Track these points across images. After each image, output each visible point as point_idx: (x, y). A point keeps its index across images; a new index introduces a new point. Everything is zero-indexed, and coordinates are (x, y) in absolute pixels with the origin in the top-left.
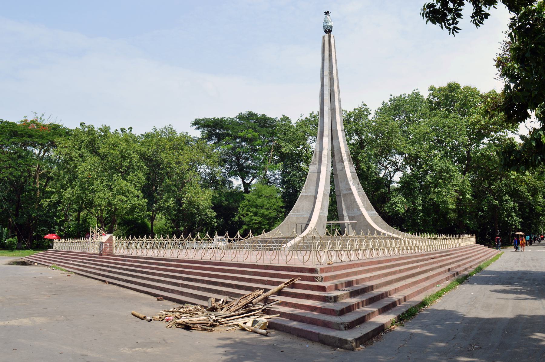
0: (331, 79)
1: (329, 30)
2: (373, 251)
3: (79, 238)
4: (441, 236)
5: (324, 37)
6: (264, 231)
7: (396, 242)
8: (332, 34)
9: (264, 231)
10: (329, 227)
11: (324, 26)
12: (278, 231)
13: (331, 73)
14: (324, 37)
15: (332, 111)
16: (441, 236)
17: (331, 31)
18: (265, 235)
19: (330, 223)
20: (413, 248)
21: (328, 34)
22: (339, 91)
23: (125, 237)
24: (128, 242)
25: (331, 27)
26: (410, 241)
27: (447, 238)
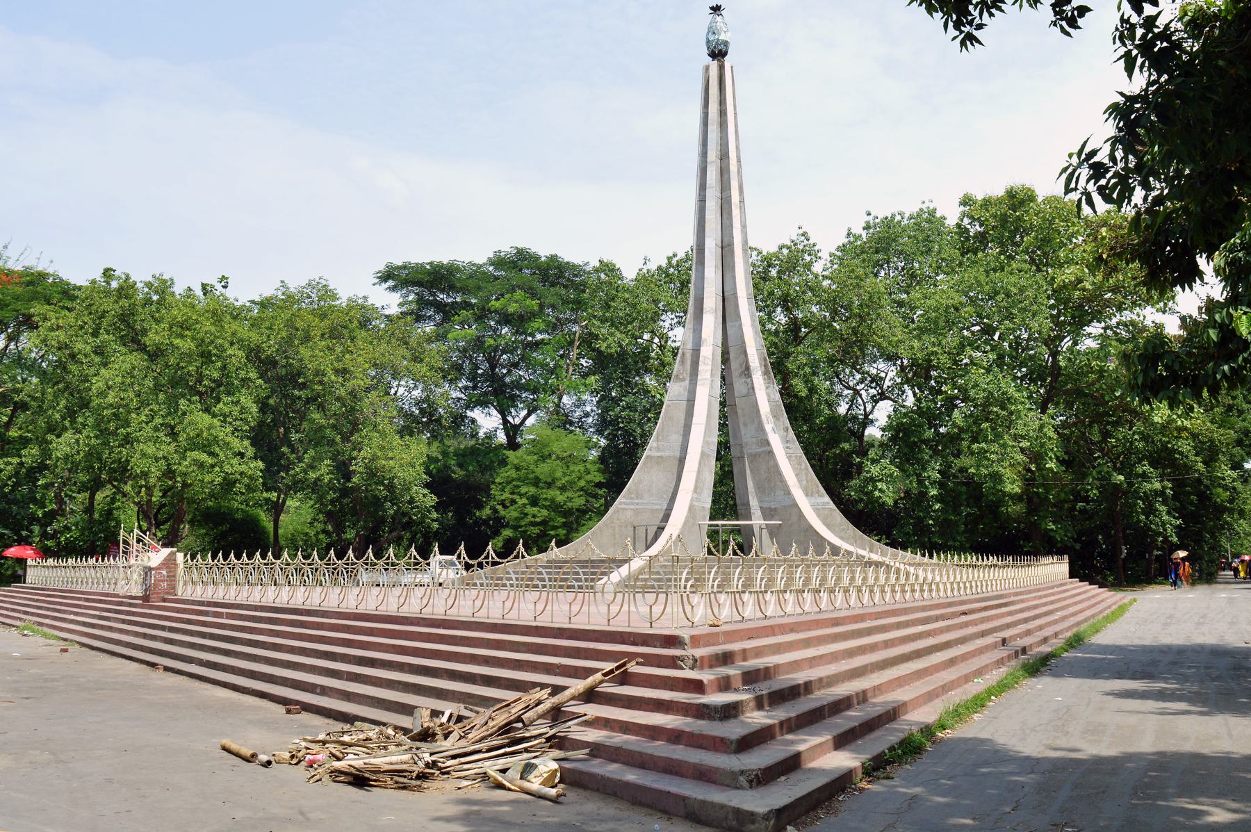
0: (724, 172)
1: (720, 51)
2: (821, 594)
3: (92, 557)
4: (985, 558)
5: (707, 68)
6: (553, 543)
7: (877, 573)
8: (728, 61)
9: (553, 543)
10: (713, 534)
11: (708, 42)
12: (588, 544)
13: (724, 156)
14: (707, 68)
15: (726, 249)
16: (985, 558)
17: (726, 53)
18: (555, 553)
19: (717, 526)
20: (917, 588)
21: (719, 60)
22: (742, 201)
23: (206, 555)
24: (215, 569)
25: (726, 43)
26: (911, 570)
27: (1000, 563)
